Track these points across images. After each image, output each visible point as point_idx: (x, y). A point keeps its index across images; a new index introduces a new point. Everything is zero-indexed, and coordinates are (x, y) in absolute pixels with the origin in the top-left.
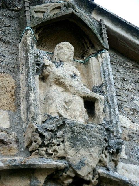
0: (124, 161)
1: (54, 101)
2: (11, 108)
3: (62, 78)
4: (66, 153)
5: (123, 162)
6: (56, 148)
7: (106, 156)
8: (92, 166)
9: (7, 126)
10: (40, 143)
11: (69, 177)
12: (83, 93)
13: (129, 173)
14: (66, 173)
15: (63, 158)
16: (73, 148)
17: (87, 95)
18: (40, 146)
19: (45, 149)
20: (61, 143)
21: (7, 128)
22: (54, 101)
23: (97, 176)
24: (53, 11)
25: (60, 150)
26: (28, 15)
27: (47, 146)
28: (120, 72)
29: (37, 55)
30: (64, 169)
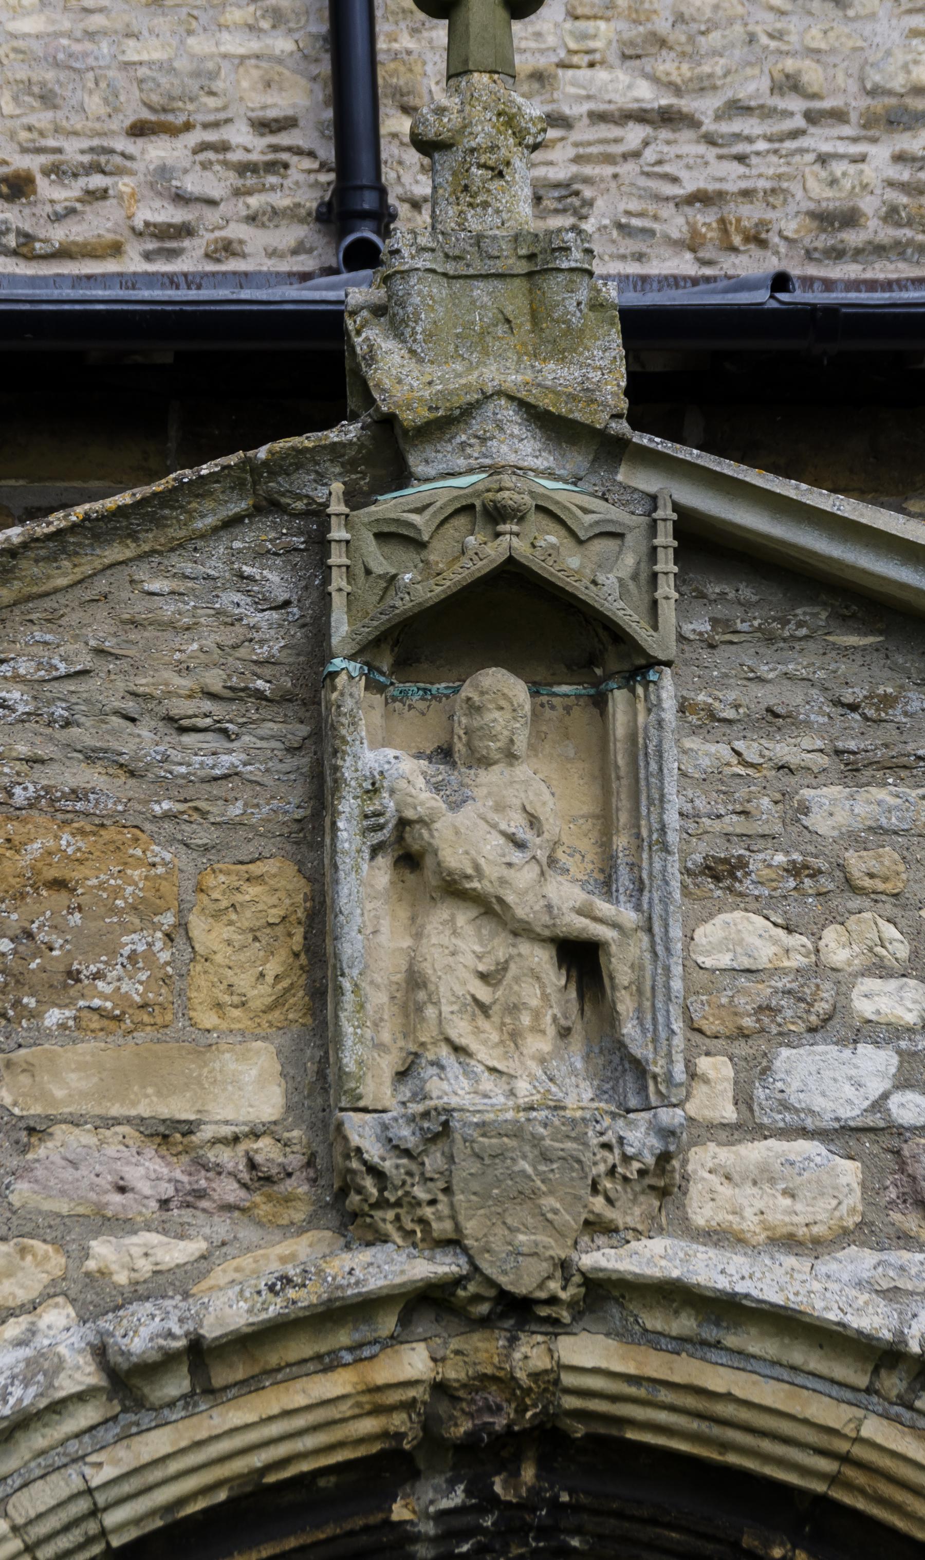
0: (723, 1135)
1: (430, 995)
2: (291, 1016)
3: (468, 877)
4: (458, 1228)
5: (720, 1144)
6: (428, 1211)
7: (610, 1201)
8: (552, 1258)
9: (270, 1110)
10: (373, 1200)
11: (477, 1298)
12: (547, 927)
13: (737, 1185)
14: (465, 1288)
15: (454, 1243)
16: (482, 1211)
17: (561, 931)
18: (377, 1205)
19: (390, 1215)
20: (441, 1197)
21: (273, 1118)
22: (430, 995)
23: (577, 1279)
24: (442, 530)
25: (440, 1219)
26: (340, 590)
27: (398, 1204)
28: (765, 675)
29: (373, 784)
30: (459, 1281)
